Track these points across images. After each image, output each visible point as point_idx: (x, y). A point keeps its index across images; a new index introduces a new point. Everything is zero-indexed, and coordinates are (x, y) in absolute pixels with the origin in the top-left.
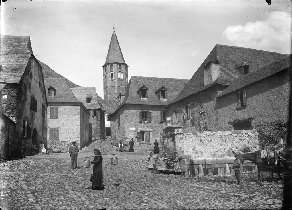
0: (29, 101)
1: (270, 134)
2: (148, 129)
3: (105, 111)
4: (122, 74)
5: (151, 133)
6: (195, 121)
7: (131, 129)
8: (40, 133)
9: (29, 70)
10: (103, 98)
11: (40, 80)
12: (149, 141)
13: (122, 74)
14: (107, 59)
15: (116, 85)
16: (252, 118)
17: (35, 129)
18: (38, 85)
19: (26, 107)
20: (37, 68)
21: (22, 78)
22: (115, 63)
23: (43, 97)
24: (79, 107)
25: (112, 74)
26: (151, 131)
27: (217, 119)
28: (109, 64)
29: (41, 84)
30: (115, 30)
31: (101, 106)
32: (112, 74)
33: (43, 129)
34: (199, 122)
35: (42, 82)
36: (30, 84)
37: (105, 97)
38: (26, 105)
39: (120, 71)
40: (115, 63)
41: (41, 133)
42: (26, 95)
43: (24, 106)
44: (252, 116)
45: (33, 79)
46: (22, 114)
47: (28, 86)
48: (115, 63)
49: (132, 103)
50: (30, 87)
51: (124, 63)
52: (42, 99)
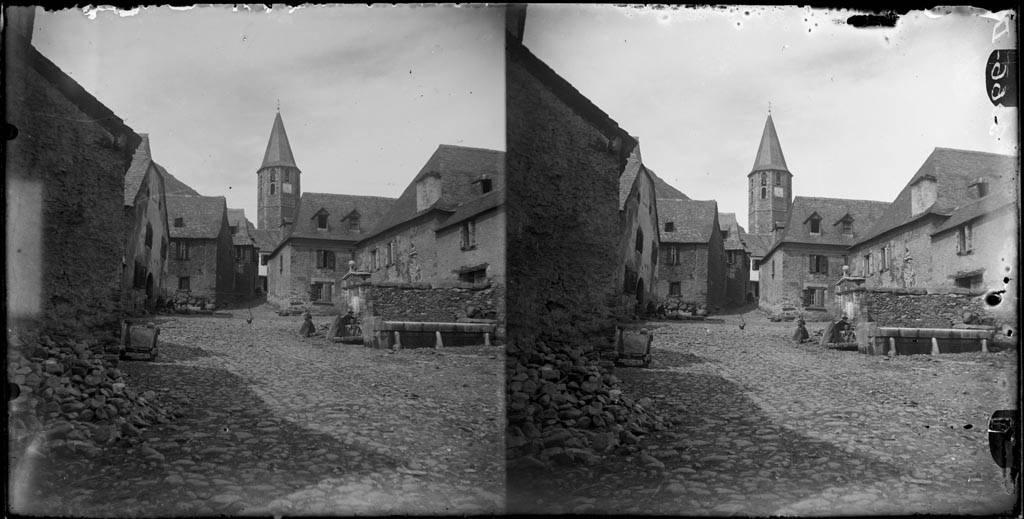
0: (144, 231)
2: (327, 280)
3: (750, 253)
4: (781, 190)
5: (826, 292)
6: (895, 273)
10: (747, 231)
12: (823, 305)
13: (781, 190)
14: (757, 162)
15: (771, 208)
16: (486, 265)
17: (151, 274)
18: (648, 211)
20: (648, 186)
21: (137, 197)
26: (825, 289)
27: (931, 270)
28: (268, 168)
29: (162, 203)
30: (773, 111)
31: (744, 244)
34: (903, 274)
35: (653, 207)
36: (146, 206)
37: (750, 229)
39: (778, 185)
40: (278, 167)
41: (649, 286)
42: (630, 228)
44: (487, 261)
48: (769, 170)
49: (795, 240)
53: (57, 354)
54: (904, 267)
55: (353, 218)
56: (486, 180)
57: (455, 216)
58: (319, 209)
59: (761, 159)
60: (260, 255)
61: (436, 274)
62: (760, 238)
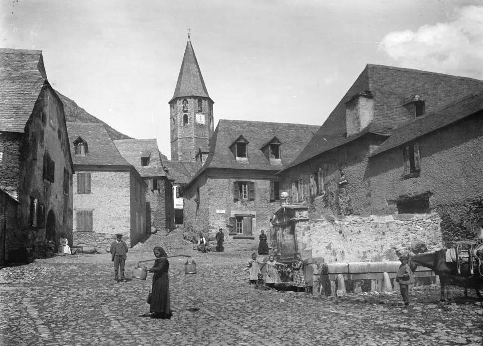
0: (40, 163)
1: (462, 220)
2: (248, 212)
3: (173, 181)
4: (203, 117)
7: (218, 211)
8: (59, 220)
9: (41, 110)
10: (169, 158)
11: (60, 127)
13: (203, 117)
14: (178, 89)
15: (193, 135)
16: (430, 193)
17: (51, 212)
18: (56, 135)
19: (36, 173)
22: (191, 97)
23: (65, 156)
24: (128, 174)
25: (186, 117)
26: (254, 216)
27: (369, 195)
29: (62, 133)
31: (167, 171)
32: (186, 117)
33: (65, 211)
34: (337, 199)
36: (42, 133)
37: (173, 157)
38: (36, 169)
39: (200, 111)
40: (190, 97)
43: (32, 171)
44: (431, 189)
45: (48, 125)
46: (29, 185)
47: (39, 138)
48: (190, 97)
50: (42, 138)
51: (206, 96)
52: (64, 159)
53: (239, 309)
54: (339, 193)
55: (273, 147)
56: (420, 101)
57: (390, 140)
58: (238, 137)
59: (182, 87)
60: (175, 187)
61: (369, 204)
62: (183, 164)
